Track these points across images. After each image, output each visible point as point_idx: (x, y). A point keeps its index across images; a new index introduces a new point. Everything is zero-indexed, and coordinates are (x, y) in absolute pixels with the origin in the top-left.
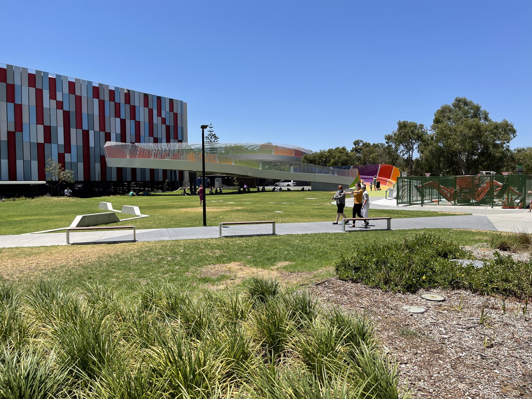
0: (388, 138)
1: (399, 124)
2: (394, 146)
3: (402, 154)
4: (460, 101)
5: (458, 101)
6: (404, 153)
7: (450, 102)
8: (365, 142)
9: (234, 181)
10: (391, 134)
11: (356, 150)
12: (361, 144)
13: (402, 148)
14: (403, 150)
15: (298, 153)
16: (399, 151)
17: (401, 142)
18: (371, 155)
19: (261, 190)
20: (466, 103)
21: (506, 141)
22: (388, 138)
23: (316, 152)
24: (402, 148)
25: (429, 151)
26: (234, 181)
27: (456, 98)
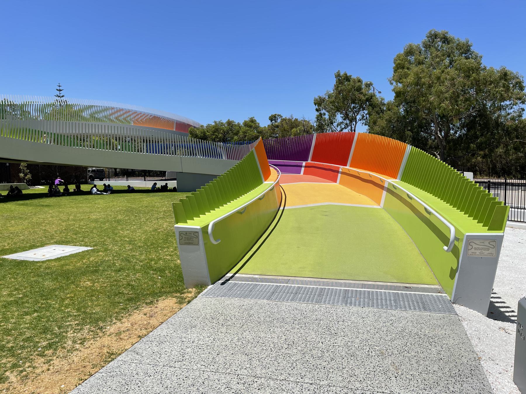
0: (319, 103)
1: (338, 76)
2: (327, 117)
3: (339, 129)
4: (436, 36)
5: (434, 36)
6: (343, 127)
7: (418, 40)
8: (284, 117)
9: (20, 171)
10: (323, 94)
11: (273, 128)
12: (279, 120)
13: (339, 117)
14: (342, 123)
15: (182, 127)
16: (335, 124)
17: (338, 109)
18: (294, 130)
19: (71, 190)
20: (446, 40)
21: (519, 102)
22: (319, 103)
23: (209, 126)
24: (339, 117)
25: (386, 120)
26: (20, 171)
27: (430, 33)
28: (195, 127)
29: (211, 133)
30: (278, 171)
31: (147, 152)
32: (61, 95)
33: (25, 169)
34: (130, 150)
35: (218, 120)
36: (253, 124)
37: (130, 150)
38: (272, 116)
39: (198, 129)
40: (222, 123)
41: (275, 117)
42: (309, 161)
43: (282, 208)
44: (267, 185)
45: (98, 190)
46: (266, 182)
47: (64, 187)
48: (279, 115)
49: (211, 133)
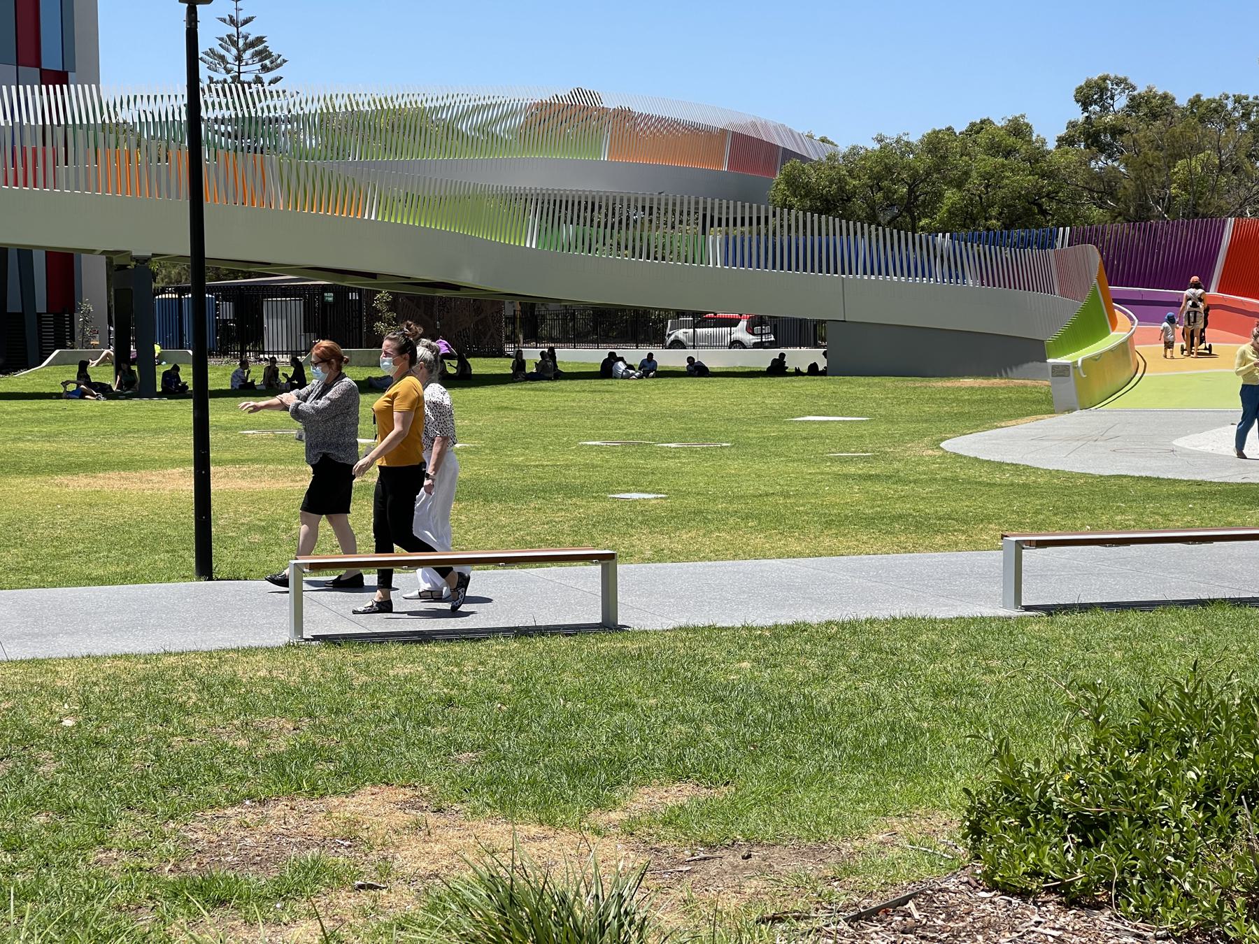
8: (1141, 89)
11: (1091, 136)
12: (1121, 102)
15: (752, 152)
23: (854, 151)
28: (803, 159)
29: (865, 179)
30: (1131, 319)
31: (774, 268)
32: (242, 17)
33: (385, 308)
34: (730, 262)
35: (891, 134)
36: (1019, 143)
37: (730, 262)
38: (1089, 85)
39: (817, 166)
40: (908, 143)
41: (1102, 90)
42: (1213, 292)
43: (1139, 375)
44: (1113, 339)
45: (630, 367)
46: (1113, 333)
47: (455, 363)
48: (1119, 82)
49: (865, 179)
